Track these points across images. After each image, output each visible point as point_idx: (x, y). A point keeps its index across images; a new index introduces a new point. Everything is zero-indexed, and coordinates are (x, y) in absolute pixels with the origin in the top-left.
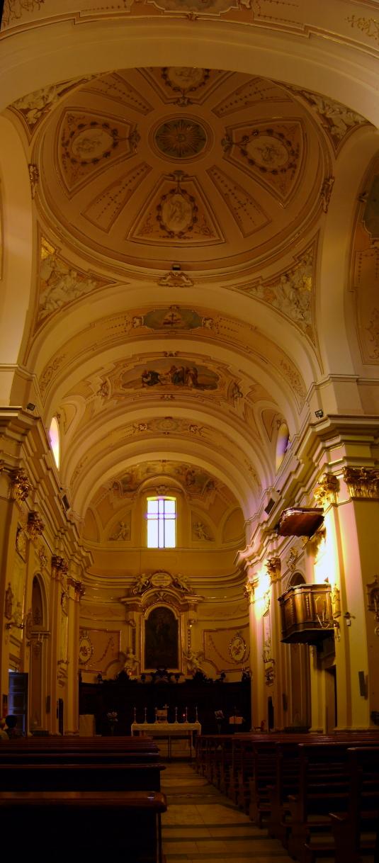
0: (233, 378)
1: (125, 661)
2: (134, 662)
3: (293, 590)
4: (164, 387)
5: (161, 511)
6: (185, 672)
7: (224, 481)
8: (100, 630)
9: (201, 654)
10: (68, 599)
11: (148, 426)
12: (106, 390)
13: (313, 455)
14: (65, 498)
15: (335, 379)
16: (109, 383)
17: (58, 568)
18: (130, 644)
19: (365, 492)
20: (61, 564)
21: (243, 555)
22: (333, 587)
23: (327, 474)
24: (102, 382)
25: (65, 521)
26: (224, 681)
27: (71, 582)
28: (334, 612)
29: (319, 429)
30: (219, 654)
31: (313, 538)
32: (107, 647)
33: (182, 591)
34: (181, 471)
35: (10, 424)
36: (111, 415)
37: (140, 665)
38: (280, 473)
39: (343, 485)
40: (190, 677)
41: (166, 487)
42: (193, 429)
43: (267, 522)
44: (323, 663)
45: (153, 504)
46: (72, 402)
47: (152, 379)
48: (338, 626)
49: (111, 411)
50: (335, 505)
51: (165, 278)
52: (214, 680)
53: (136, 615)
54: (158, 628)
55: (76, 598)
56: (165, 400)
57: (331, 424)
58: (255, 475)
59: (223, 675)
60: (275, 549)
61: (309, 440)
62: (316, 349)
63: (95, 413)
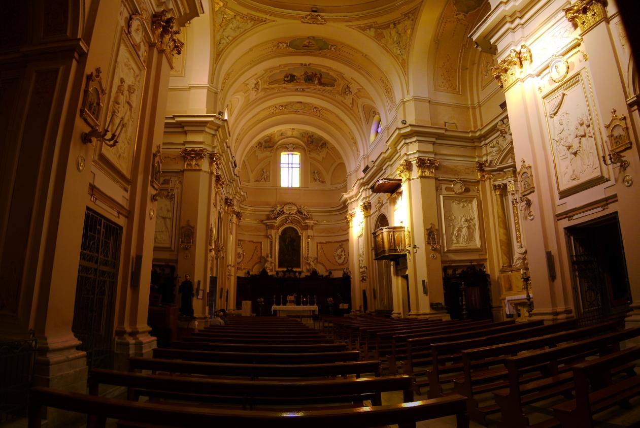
0: (346, 82)
1: (265, 263)
2: (272, 263)
3: (382, 229)
4: (298, 84)
5: (290, 162)
6: (305, 270)
7: (333, 143)
8: (249, 241)
9: (316, 259)
10: (233, 223)
11: (284, 108)
12: (257, 87)
13: (398, 145)
14: (235, 163)
15: (416, 99)
16: (260, 83)
17: (229, 205)
18: (269, 252)
19: (427, 173)
20: (230, 203)
21: (346, 196)
22: (406, 229)
23: (406, 160)
24: (256, 82)
25: (233, 175)
26: (331, 277)
27: (234, 212)
28: (407, 244)
29: (403, 131)
30: (327, 259)
31: (394, 195)
32: (254, 253)
33: (304, 216)
34: (304, 135)
35: (208, 125)
36: (260, 101)
37: (275, 265)
38: (373, 146)
39: (415, 168)
40: (309, 274)
41: (293, 145)
42: (315, 110)
43: (363, 178)
44: (399, 272)
45: (285, 157)
46: (236, 97)
47: (291, 78)
48: (409, 252)
49: (260, 99)
50: (409, 180)
51: (306, 18)
52: (324, 276)
53: (273, 232)
54: (287, 240)
55: (237, 222)
56: (298, 91)
57: (411, 130)
58: (355, 143)
59: (330, 273)
60: (368, 195)
61: (397, 136)
62: (406, 77)
63: (250, 101)
